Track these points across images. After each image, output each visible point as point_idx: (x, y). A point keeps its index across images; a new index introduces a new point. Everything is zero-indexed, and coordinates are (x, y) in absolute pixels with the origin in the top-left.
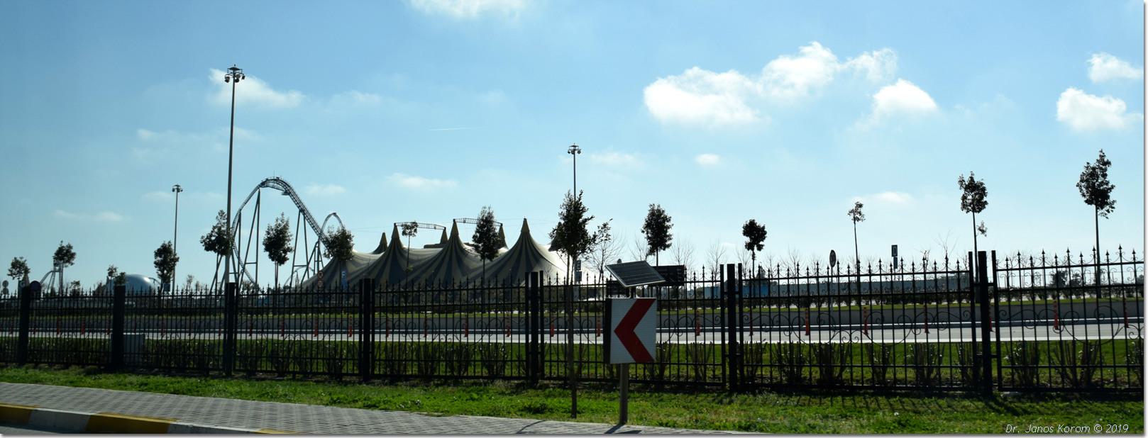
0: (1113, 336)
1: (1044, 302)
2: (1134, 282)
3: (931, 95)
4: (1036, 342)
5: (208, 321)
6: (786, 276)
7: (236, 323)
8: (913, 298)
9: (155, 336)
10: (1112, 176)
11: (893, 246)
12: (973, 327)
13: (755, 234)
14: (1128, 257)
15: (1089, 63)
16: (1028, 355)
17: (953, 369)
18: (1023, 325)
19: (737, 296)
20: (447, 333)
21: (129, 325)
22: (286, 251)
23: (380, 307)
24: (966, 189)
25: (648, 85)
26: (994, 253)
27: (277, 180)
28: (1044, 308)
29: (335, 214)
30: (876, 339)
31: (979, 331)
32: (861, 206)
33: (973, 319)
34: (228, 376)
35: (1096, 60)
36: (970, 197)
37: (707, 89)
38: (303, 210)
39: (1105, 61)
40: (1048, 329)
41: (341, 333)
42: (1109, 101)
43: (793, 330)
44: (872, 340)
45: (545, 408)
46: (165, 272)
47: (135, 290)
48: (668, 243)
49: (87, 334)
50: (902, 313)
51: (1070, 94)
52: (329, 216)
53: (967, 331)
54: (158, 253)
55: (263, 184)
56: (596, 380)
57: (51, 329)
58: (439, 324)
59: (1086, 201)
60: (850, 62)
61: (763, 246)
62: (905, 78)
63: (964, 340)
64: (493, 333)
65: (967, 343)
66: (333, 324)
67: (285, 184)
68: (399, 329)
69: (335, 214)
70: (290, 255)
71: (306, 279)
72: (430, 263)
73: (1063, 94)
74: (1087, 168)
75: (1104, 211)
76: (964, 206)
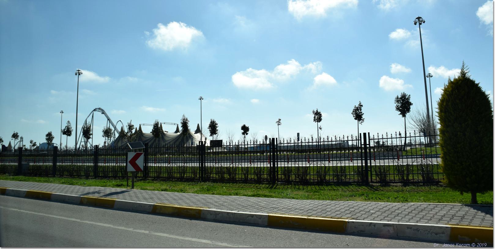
0: (310, 165)
1: (256, 155)
2: (373, 146)
3: (335, 78)
4: (380, 166)
5: (48, 159)
6: (286, 143)
7: (148, 159)
8: (305, 151)
9: (31, 164)
10: (363, 110)
11: (298, 133)
12: (362, 160)
13: (245, 129)
14: (389, 136)
15: (391, 67)
16: (288, 170)
17: (315, 175)
18: (380, 159)
19: (276, 149)
20: (120, 163)
21: (59, 160)
22: (90, 135)
23: (242, 151)
24: (315, 114)
25: (233, 74)
26: (369, 133)
27: (99, 109)
28: (344, 154)
29: (120, 121)
30: (355, 164)
31: (364, 161)
32: (280, 120)
33: (362, 157)
34: (54, 176)
35: (393, 66)
36: (316, 117)
37: (255, 76)
38: (109, 119)
39: (396, 66)
40: (437, 159)
41: (114, 163)
42: (398, 80)
43: (219, 162)
44: (242, 165)
45: (122, 185)
46: (49, 142)
47: (45, 148)
48: (217, 132)
49: (10, 163)
50: (336, 156)
51: (384, 78)
52: (118, 121)
53: (360, 161)
54: (47, 135)
55: (95, 110)
56: (163, 178)
57: (67, 162)
58: (233, 158)
59: (355, 119)
60: (306, 66)
61: (248, 133)
62: (325, 72)
63: (303, 166)
64: (188, 163)
65: (373, 166)
66: (86, 160)
67: (102, 110)
68: (224, 161)
69: (120, 121)
70: (91, 136)
71: (110, 143)
72: (151, 139)
73: (382, 78)
74: (355, 107)
75: (361, 122)
76: (314, 120)
